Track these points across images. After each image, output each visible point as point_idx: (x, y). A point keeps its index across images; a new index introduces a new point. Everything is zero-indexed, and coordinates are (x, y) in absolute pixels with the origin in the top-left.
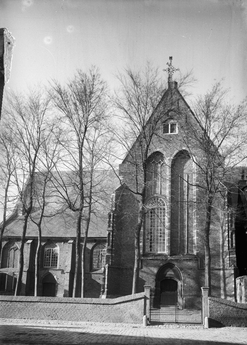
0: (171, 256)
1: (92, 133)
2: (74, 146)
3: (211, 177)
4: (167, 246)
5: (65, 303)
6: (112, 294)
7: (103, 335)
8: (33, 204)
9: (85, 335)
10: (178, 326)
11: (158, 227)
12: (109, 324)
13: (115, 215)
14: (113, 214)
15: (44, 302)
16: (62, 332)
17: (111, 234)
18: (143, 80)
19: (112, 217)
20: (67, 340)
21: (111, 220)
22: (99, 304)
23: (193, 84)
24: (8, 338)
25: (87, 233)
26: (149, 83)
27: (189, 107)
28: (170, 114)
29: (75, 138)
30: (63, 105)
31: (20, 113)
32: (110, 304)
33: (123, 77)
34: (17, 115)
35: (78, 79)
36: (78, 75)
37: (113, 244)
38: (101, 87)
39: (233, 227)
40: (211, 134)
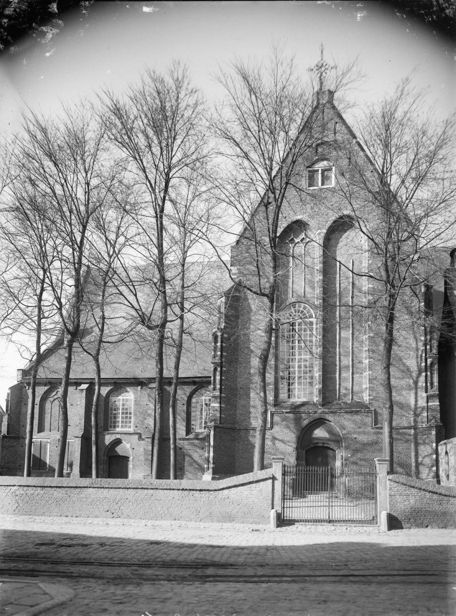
0: (323, 405)
1: (180, 189)
2: (148, 216)
3: (393, 259)
4: (317, 389)
5: (134, 488)
6: (222, 473)
7: (192, 546)
8: (83, 318)
9: (159, 546)
10: (333, 528)
11: (301, 355)
12: (211, 524)
13: (225, 336)
14: (222, 335)
15: (98, 488)
16: (119, 540)
17: (219, 369)
18: (267, 85)
19: (219, 340)
20: (122, 556)
21: (219, 344)
22: (193, 490)
23: (360, 85)
24: (17, 551)
25: (177, 367)
26: (280, 86)
27: (355, 137)
28: (320, 150)
29: (148, 197)
30: (126, 139)
31: (50, 156)
32: (211, 491)
33: (229, 78)
34: (48, 163)
35: (150, 89)
36: (148, 80)
37: (223, 387)
38: (191, 101)
39: (435, 351)
40: (395, 177)
